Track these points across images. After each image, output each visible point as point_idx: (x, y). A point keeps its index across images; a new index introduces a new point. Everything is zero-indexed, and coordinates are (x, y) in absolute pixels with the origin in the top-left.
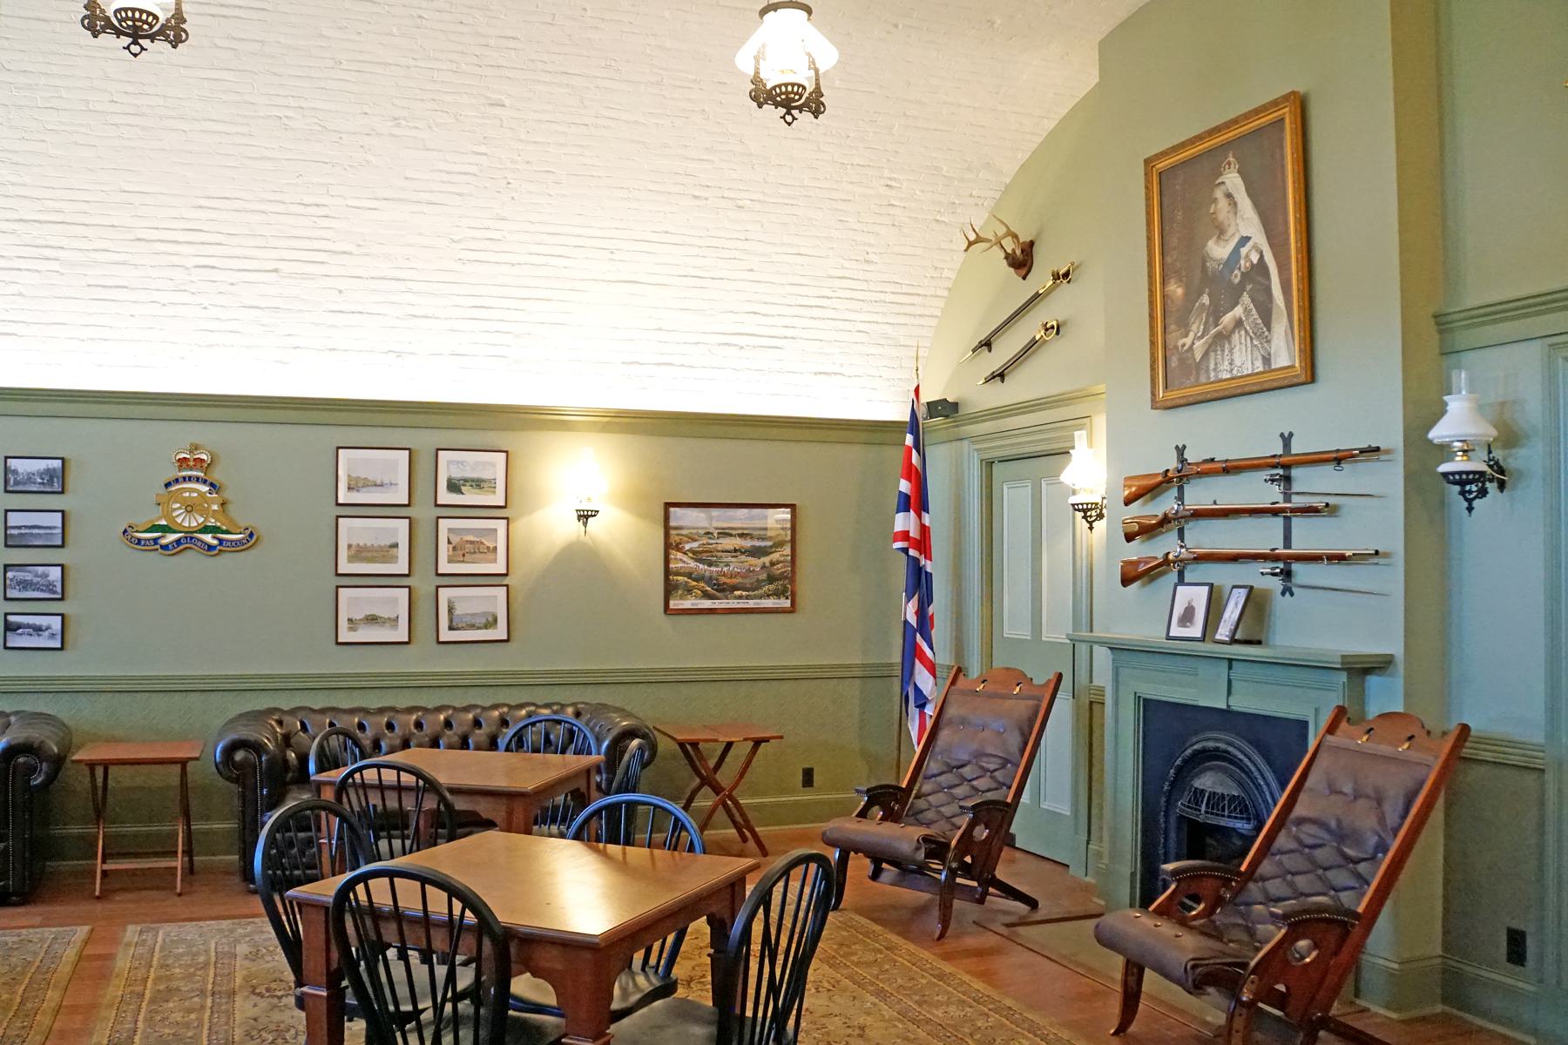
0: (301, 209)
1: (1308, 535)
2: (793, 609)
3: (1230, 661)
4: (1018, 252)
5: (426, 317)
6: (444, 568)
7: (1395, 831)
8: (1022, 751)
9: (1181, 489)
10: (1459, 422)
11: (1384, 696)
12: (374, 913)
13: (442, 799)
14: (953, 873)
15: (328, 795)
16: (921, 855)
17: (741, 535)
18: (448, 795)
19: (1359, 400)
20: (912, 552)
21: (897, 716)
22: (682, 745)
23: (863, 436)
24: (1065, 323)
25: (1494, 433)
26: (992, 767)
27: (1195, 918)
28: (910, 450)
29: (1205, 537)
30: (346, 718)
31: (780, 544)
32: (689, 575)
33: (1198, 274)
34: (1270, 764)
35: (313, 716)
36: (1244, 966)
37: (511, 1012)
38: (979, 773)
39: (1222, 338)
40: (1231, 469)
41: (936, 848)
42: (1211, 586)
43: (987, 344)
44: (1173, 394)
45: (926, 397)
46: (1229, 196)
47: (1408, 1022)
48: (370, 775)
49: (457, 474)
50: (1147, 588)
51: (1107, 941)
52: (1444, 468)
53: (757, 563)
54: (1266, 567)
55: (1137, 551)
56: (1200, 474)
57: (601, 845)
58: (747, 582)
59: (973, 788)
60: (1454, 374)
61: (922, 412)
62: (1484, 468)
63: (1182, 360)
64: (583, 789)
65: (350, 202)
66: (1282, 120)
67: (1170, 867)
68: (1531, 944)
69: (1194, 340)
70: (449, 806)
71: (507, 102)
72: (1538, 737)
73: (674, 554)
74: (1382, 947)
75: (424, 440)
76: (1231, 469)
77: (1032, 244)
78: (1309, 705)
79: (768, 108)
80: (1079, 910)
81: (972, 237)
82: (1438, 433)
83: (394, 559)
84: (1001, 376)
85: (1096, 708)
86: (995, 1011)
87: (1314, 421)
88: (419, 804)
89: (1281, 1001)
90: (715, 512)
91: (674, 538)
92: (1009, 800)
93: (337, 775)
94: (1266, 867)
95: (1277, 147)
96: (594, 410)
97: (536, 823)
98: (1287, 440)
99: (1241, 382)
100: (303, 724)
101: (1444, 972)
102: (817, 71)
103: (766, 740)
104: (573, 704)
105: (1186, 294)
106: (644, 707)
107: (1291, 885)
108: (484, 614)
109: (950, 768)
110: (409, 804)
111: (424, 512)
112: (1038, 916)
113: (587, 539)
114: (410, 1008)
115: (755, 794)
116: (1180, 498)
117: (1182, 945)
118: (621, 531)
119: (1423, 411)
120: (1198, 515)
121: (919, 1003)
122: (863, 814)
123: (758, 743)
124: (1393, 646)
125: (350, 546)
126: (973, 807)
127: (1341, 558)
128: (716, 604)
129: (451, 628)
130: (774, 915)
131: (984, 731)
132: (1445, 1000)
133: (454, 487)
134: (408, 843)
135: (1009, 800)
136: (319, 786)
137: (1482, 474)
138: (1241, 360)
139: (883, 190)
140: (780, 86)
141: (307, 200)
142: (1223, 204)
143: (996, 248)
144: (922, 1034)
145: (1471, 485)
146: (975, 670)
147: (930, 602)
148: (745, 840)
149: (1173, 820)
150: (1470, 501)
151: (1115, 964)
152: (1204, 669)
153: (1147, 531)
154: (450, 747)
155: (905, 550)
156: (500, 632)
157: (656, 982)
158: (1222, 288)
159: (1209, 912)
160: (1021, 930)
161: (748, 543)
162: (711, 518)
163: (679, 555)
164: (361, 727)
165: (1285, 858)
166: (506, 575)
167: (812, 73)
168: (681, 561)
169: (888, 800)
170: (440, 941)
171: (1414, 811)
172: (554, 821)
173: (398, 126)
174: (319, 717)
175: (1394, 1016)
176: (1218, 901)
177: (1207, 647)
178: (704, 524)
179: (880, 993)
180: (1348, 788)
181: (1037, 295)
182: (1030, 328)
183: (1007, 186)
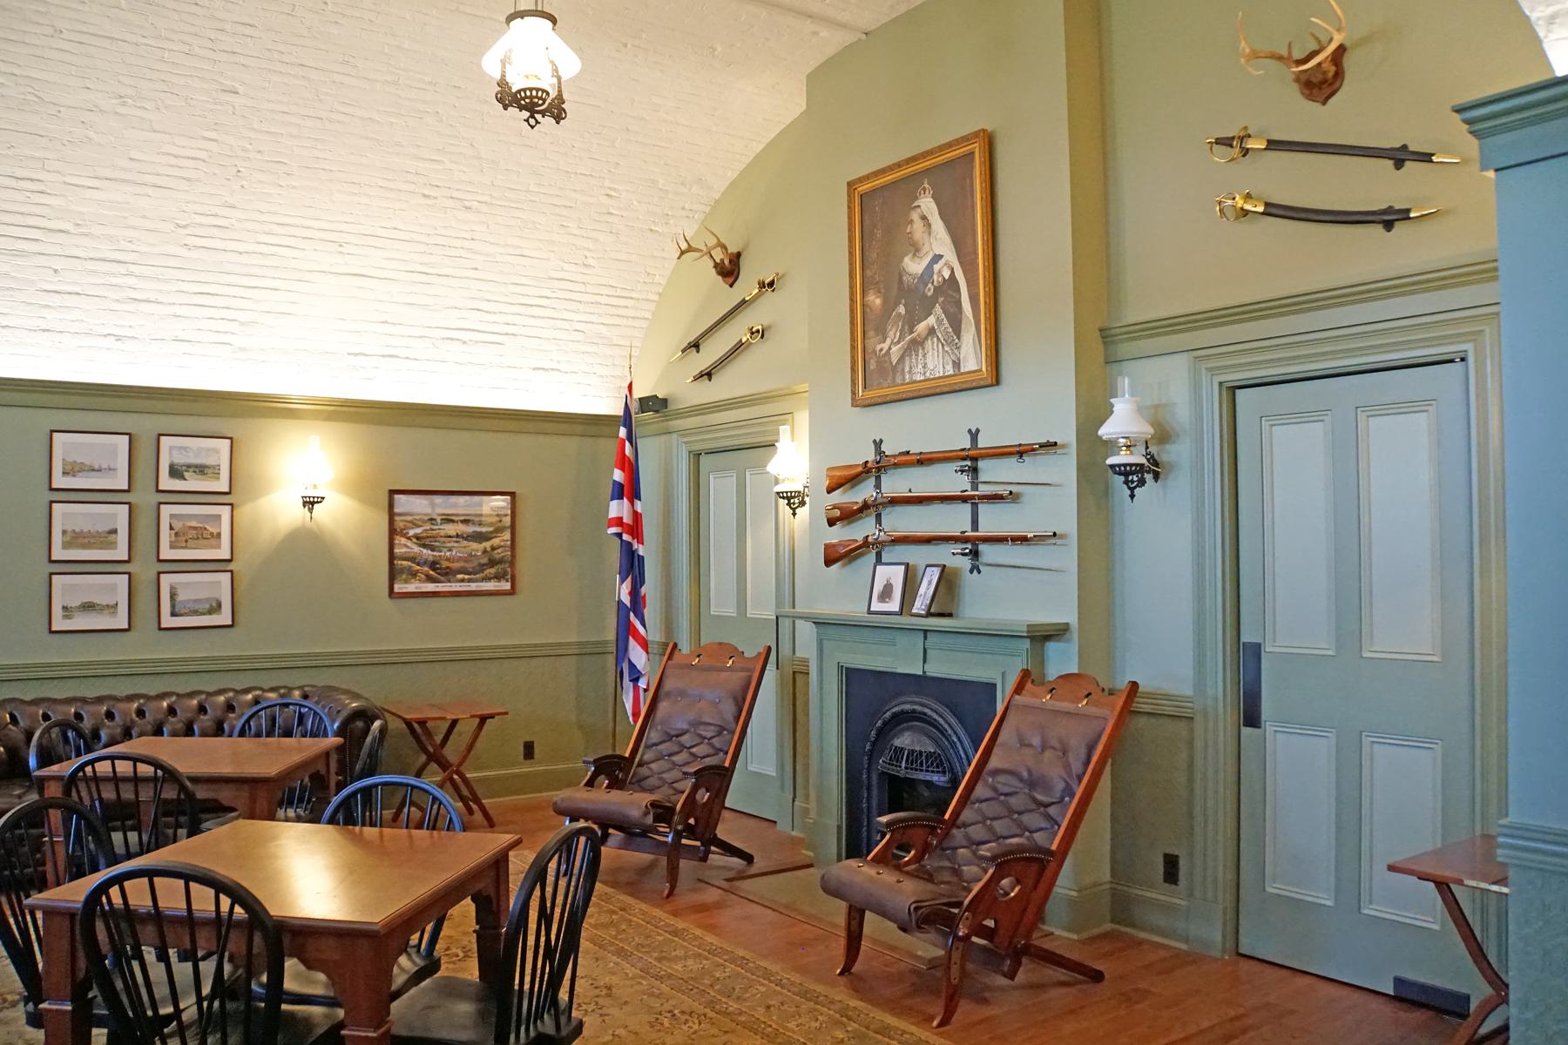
0: (12, 183)
1: (993, 520)
2: (512, 592)
3: (926, 631)
4: (727, 262)
5: (148, 301)
6: (166, 553)
7: (1080, 779)
8: (737, 718)
9: (878, 478)
10: (1123, 422)
11: (1061, 660)
12: (128, 913)
13: (183, 788)
14: (678, 835)
15: (53, 790)
16: (650, 820)
17: (465, 522)
18: (188, 784)
19: (1036, 400)
20: (626, 537)
21: (612, 690)
22: (408, 723)
23: (579, 428)
24: (769, 327)
25: (1152, 431)
26: (709, 735)
27: (908, 863)
28: (623, 441)
29: (901, 521)
30: (62, 708)
31: (499, 530)
32: (412, 559)
33: (895, 286)
34: (961, 721)
35: (88, 708)
36: (958, 904)
37: (284, 1007)
38: (698, 740)
39: (917, 344)
40: (924, 460)
41: (663, 813)
42: (907, 565)
43: (696, 345)
44: (870, 394)
45: (638, 393)
46: (924, 218)
47: (1083, 942)
48: (104, 768)
49: (180, 459)
50: (849, 567)
51: (832, 889)
52: (1110, 461)
53: (477, 547)
54: (957, 548)
55: (838, 534)
56: (896, 466)
57: (357, 829)
58: (469, 566)
59: (693, 755)
60: (1119, 379)
61: (634, 407)
62: (1144, 461)
63: (879, 363)
64: (323, 772)
65: (68, 180)
66: (972, 153)
67: (884, 819)
68: (1183, 865)
69: (891, 345)
70: (190, 796)
71: (241, 89)
72: (1189, 692)
73: (400, 540)
74: (1065, 884)
75: (145, 425)
76: (924, 460)
77: (739, 255)
78: (998, 670)
79: (513, 111)
80: (788, 861)
81: (684, 246)
82: (1106, 431)
83: (112, 545)
84: (708, 374)
85: (799, 677)
86: (732, 961)
87: (998, 418)
88: (157, 794)
89: (988, 934)
90: (438, 499)
91: (400, 523)
92: (727, 764)
93: (65, 769)
94: (967, 815)
95: (967, 174)
96: (314, 398)
97: (280, 805)
98: (974, 435)
99: (932, 383)
100: (13, 717)
101: (1113, 895)
102: (559, 79)
103: (492, 716)
104: (301, 688)
105: (885, 302)
106: (373, 689)
107: (990, 829)
108: (208, 600)
109: (669, 737)
110: (146, 794)
111: (144, 497)
112: (753, 870)
113: (312, 525)
114: (170, 1010)
115: (477, 769)
116: (878, 486)
117: (905, 891)
118: (343, 514)
119: (1093, 412)
120: (894, 501)
121: (659, 960)
122: (590, 784)
123: (483, 719)
124: (1069, 616)
125: (64, 532)
126: (696, 773)
127: (1024, 539)
128: (440, 587)
129: (173, 614)
130: (549, 889)
131: (701, 702)
132: (1113, 921)
133: (175, 472)
134: (145, 838)
135: (727, 764)
136: (41, 783)
137: (1142, 465)
138: (933, 364)
139: (604, 199)
140: (524, 90)
141: (20, 173)
142: (918, 225)
143: (706, 258)
144: (665, 988)
145: (1133, 475)
146: (685, 648)
147: (642, 583)
148: (471, 812)
149: (874, 777)
150: (1132, 489)
151: (837, 911)
152: (902, 640)
153: (846, 516)
154: (174, 734)
155: (619, 535)
156: (224, 618)
157: (421, 962)
158: (917, 299)
159: (918, 859)
160: (737, 883)
161: (470, 529)
162: (433, 505)
163: (403, 540)
164: (78, 716)
165: (984, 805)
166: (230, 561)
167: (555, 81)
168: (404, 547)
169: (613, 770)
170: (205, 940)
171: (1095, 759)
172: (290, 804)
173: (124, 104)
174: (33, 709)
175: (1075, 937)
176: (925, 849)
177: (905, 620)
178: (429, 511)
179: (620, 952)
180: (1036, 741)
181: (744, 302)
182: (737, 331)
183: (717, 202)
